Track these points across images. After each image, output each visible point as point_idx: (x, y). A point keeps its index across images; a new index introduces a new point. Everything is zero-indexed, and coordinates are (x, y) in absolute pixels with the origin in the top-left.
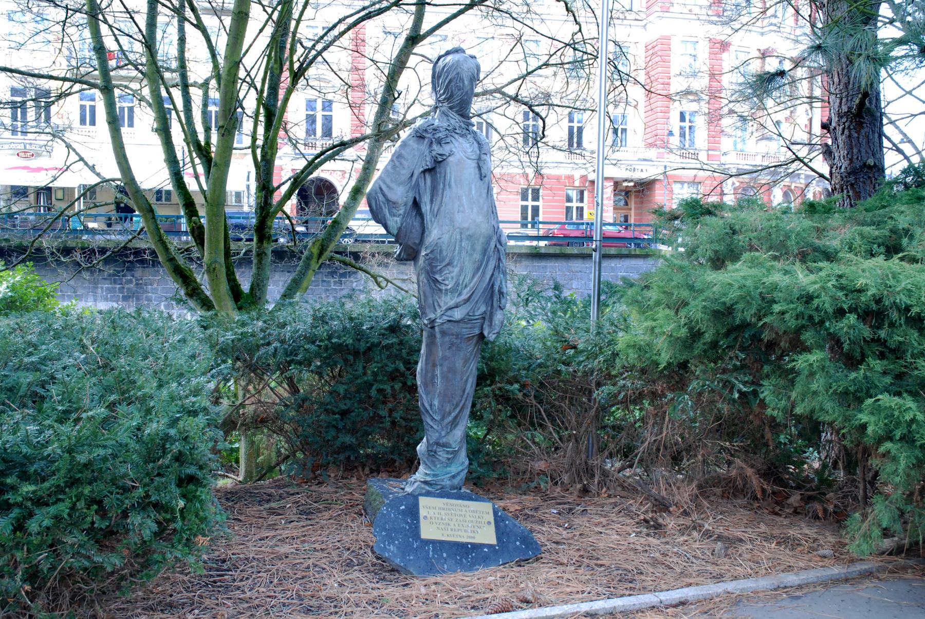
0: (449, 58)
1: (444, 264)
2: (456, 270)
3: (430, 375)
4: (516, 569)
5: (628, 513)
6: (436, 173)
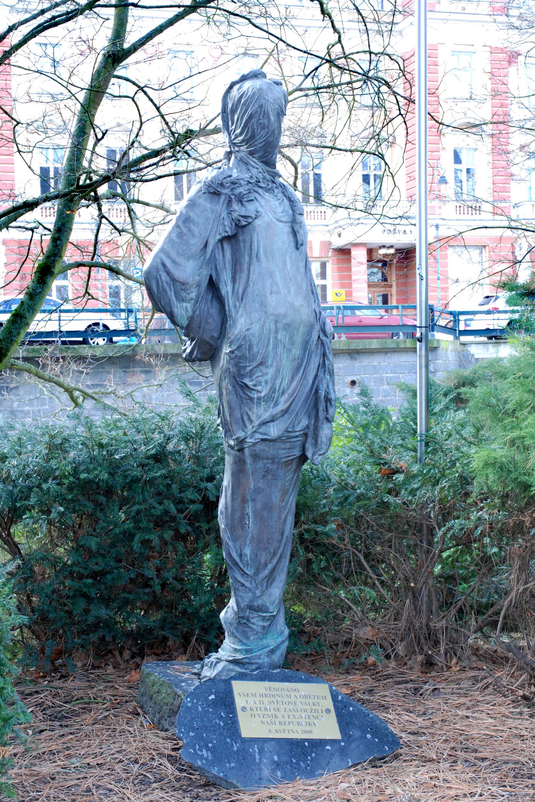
0: (247, 85)
1: (255, 364)
2: (271, 371)
3: (238, 514)
4: (371, 770)
5: (499, 690)
6: (238, 242)
